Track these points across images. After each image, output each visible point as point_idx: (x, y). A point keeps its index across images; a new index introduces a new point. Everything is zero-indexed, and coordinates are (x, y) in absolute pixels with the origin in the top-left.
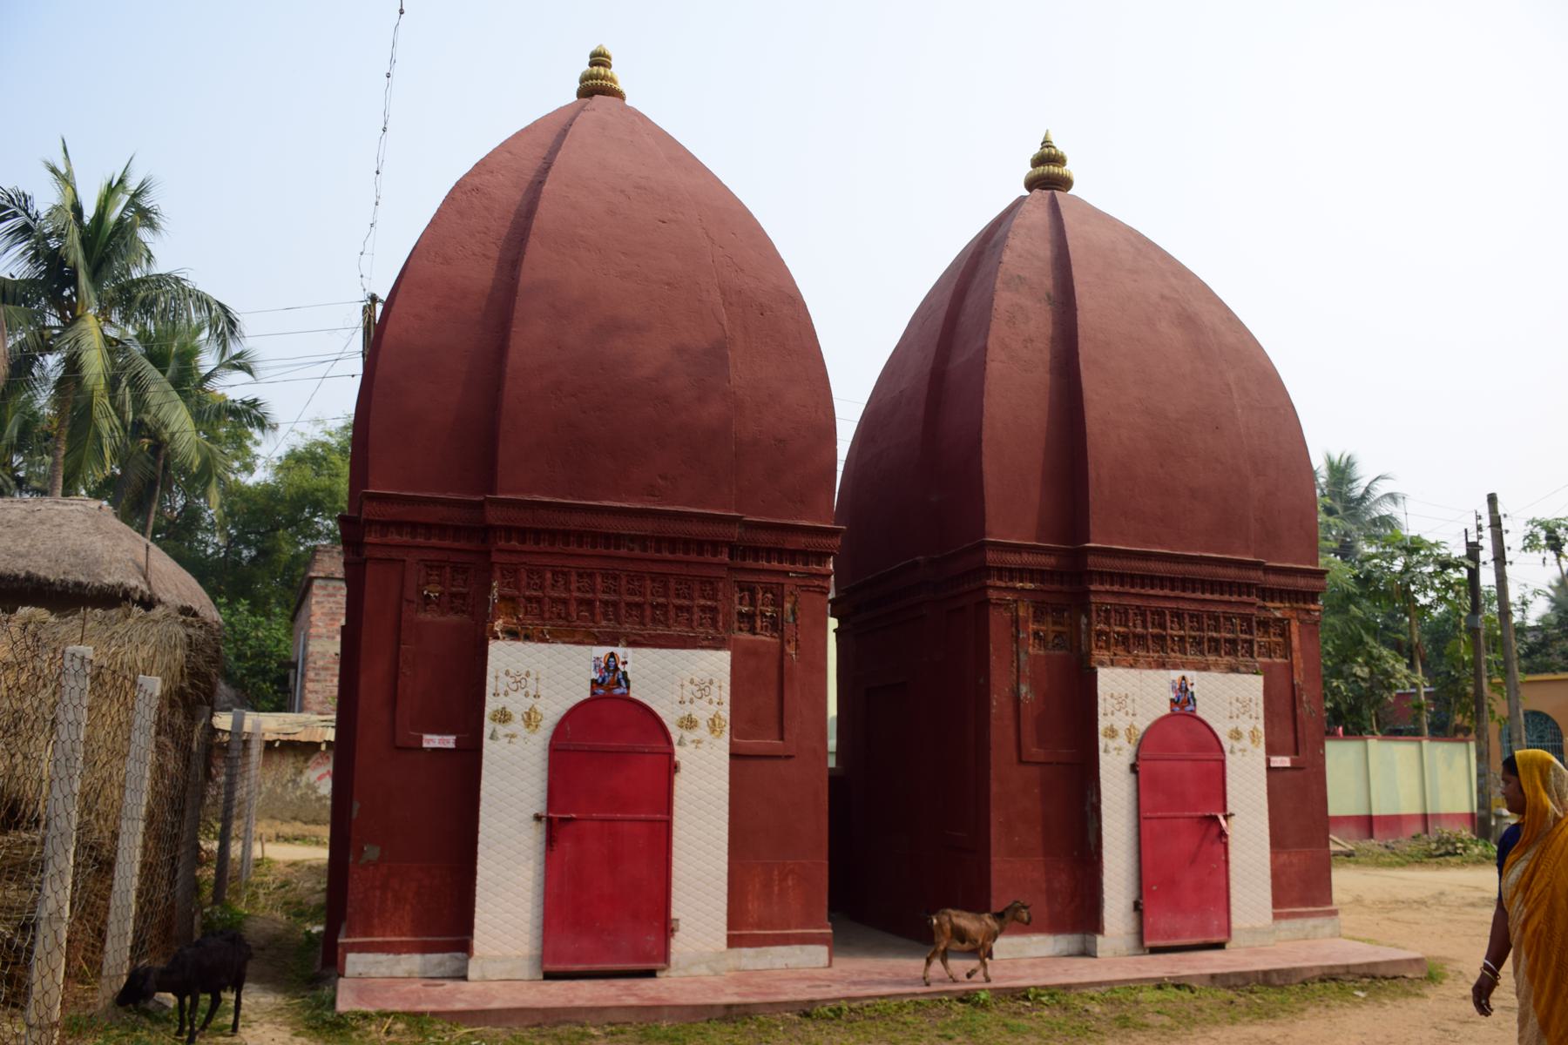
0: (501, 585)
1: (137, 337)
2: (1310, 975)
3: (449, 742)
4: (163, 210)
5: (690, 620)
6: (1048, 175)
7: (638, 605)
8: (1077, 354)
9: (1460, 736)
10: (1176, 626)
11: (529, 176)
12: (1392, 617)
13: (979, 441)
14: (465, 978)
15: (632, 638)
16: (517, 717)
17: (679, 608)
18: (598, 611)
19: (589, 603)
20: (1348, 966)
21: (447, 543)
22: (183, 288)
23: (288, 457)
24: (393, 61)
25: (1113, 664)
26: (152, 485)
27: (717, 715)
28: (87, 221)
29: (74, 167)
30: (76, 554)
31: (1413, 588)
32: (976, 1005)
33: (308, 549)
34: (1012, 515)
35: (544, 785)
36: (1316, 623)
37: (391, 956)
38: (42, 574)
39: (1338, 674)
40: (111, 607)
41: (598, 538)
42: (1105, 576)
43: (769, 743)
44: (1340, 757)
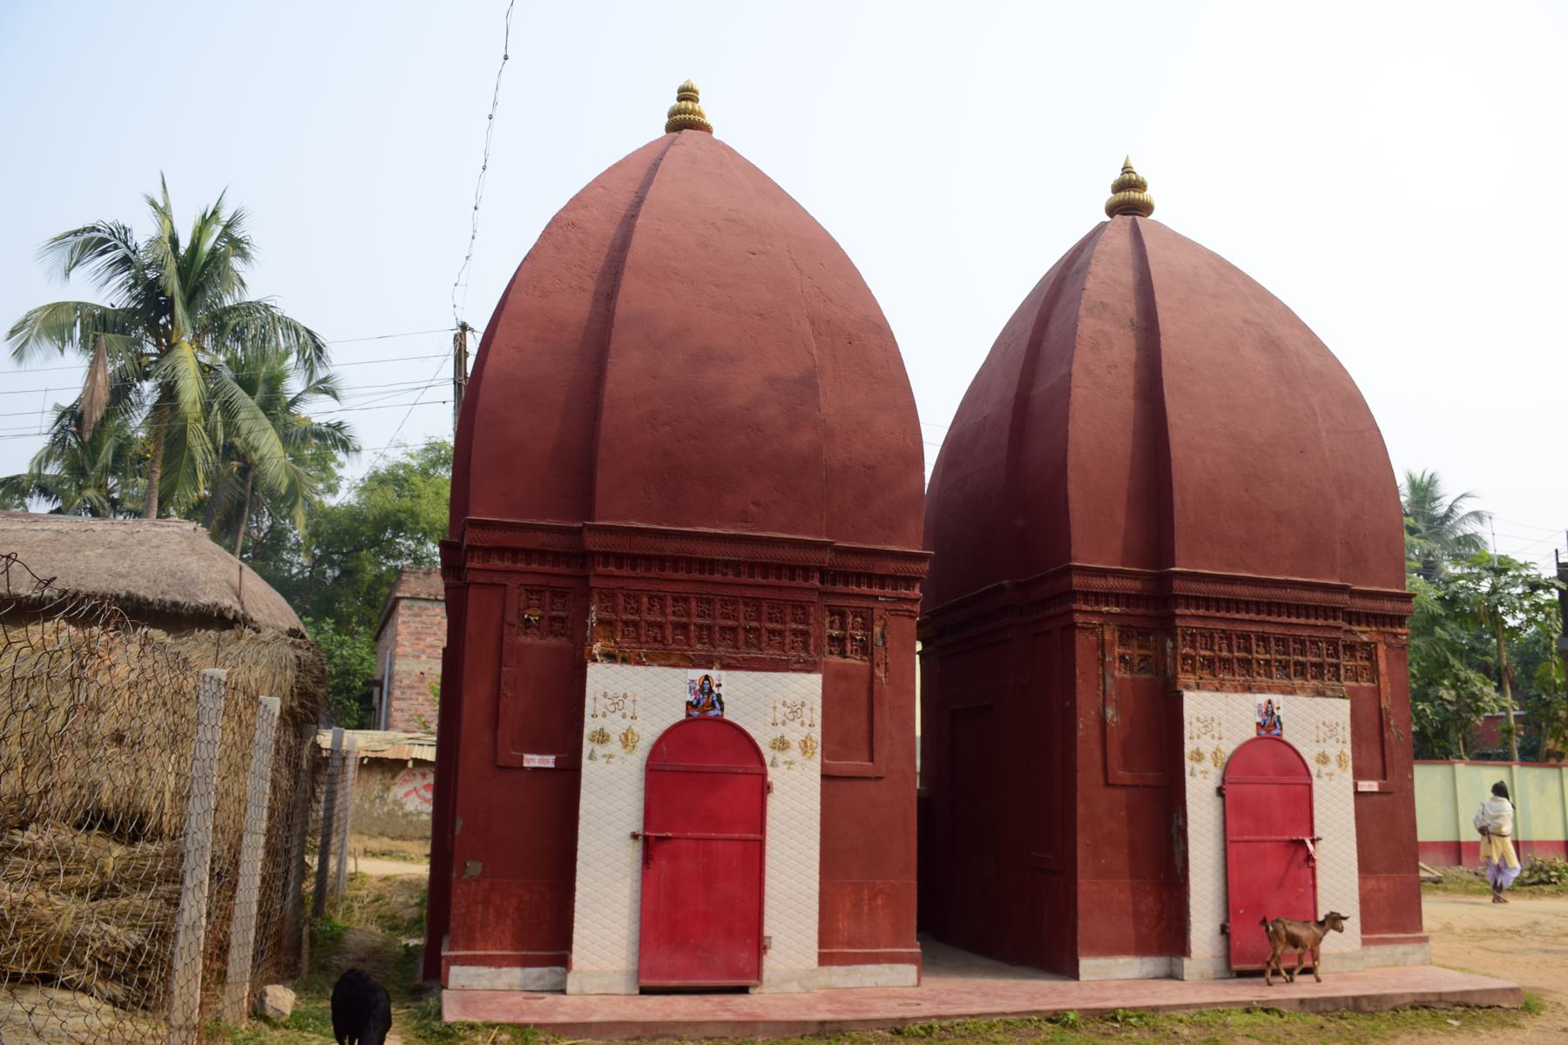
0: (599, 609)
1: (228, 362)
2: (1400, 1002)
3: (548, 761)
4: (254, 240)
5: (782, 644)
6: (1129, 201)
7: (733, 629)
8: (1161, 380)
9: (1553, 761)
10: (1261, 650)
11: (622, 210)
12: (1478, 638)
13: (1065, 466)
14: (563, 992)
15: (726, 661)
16: (615, 738)
17: (772, 632)
18: (692, 635)
19: (684, 627)
20: (1440, 994)
21: (547, 568)
22: (272, 315)
23: (371, 479)
24: (495, 103)
25: (1198, 687)
26: (241, 505)
27: (808, 737)
28: (182, 251)
29: (172, 201)
30: (173, 575)
31: (1501, 609)
32: (1065, 1025)
33: (390, 569)
34: (1098, 539)
35: (640, 805)
36: (1403, 647)
37: (493, 969)
38: (141, 593)
39: (1424, 697)
40: (224, 629)
41: (691, 563)
42: (1189, 600)
43: (858, 764)
44: (1428, 781)
